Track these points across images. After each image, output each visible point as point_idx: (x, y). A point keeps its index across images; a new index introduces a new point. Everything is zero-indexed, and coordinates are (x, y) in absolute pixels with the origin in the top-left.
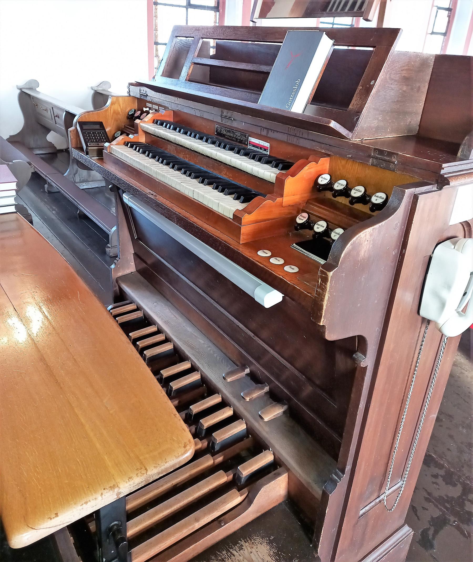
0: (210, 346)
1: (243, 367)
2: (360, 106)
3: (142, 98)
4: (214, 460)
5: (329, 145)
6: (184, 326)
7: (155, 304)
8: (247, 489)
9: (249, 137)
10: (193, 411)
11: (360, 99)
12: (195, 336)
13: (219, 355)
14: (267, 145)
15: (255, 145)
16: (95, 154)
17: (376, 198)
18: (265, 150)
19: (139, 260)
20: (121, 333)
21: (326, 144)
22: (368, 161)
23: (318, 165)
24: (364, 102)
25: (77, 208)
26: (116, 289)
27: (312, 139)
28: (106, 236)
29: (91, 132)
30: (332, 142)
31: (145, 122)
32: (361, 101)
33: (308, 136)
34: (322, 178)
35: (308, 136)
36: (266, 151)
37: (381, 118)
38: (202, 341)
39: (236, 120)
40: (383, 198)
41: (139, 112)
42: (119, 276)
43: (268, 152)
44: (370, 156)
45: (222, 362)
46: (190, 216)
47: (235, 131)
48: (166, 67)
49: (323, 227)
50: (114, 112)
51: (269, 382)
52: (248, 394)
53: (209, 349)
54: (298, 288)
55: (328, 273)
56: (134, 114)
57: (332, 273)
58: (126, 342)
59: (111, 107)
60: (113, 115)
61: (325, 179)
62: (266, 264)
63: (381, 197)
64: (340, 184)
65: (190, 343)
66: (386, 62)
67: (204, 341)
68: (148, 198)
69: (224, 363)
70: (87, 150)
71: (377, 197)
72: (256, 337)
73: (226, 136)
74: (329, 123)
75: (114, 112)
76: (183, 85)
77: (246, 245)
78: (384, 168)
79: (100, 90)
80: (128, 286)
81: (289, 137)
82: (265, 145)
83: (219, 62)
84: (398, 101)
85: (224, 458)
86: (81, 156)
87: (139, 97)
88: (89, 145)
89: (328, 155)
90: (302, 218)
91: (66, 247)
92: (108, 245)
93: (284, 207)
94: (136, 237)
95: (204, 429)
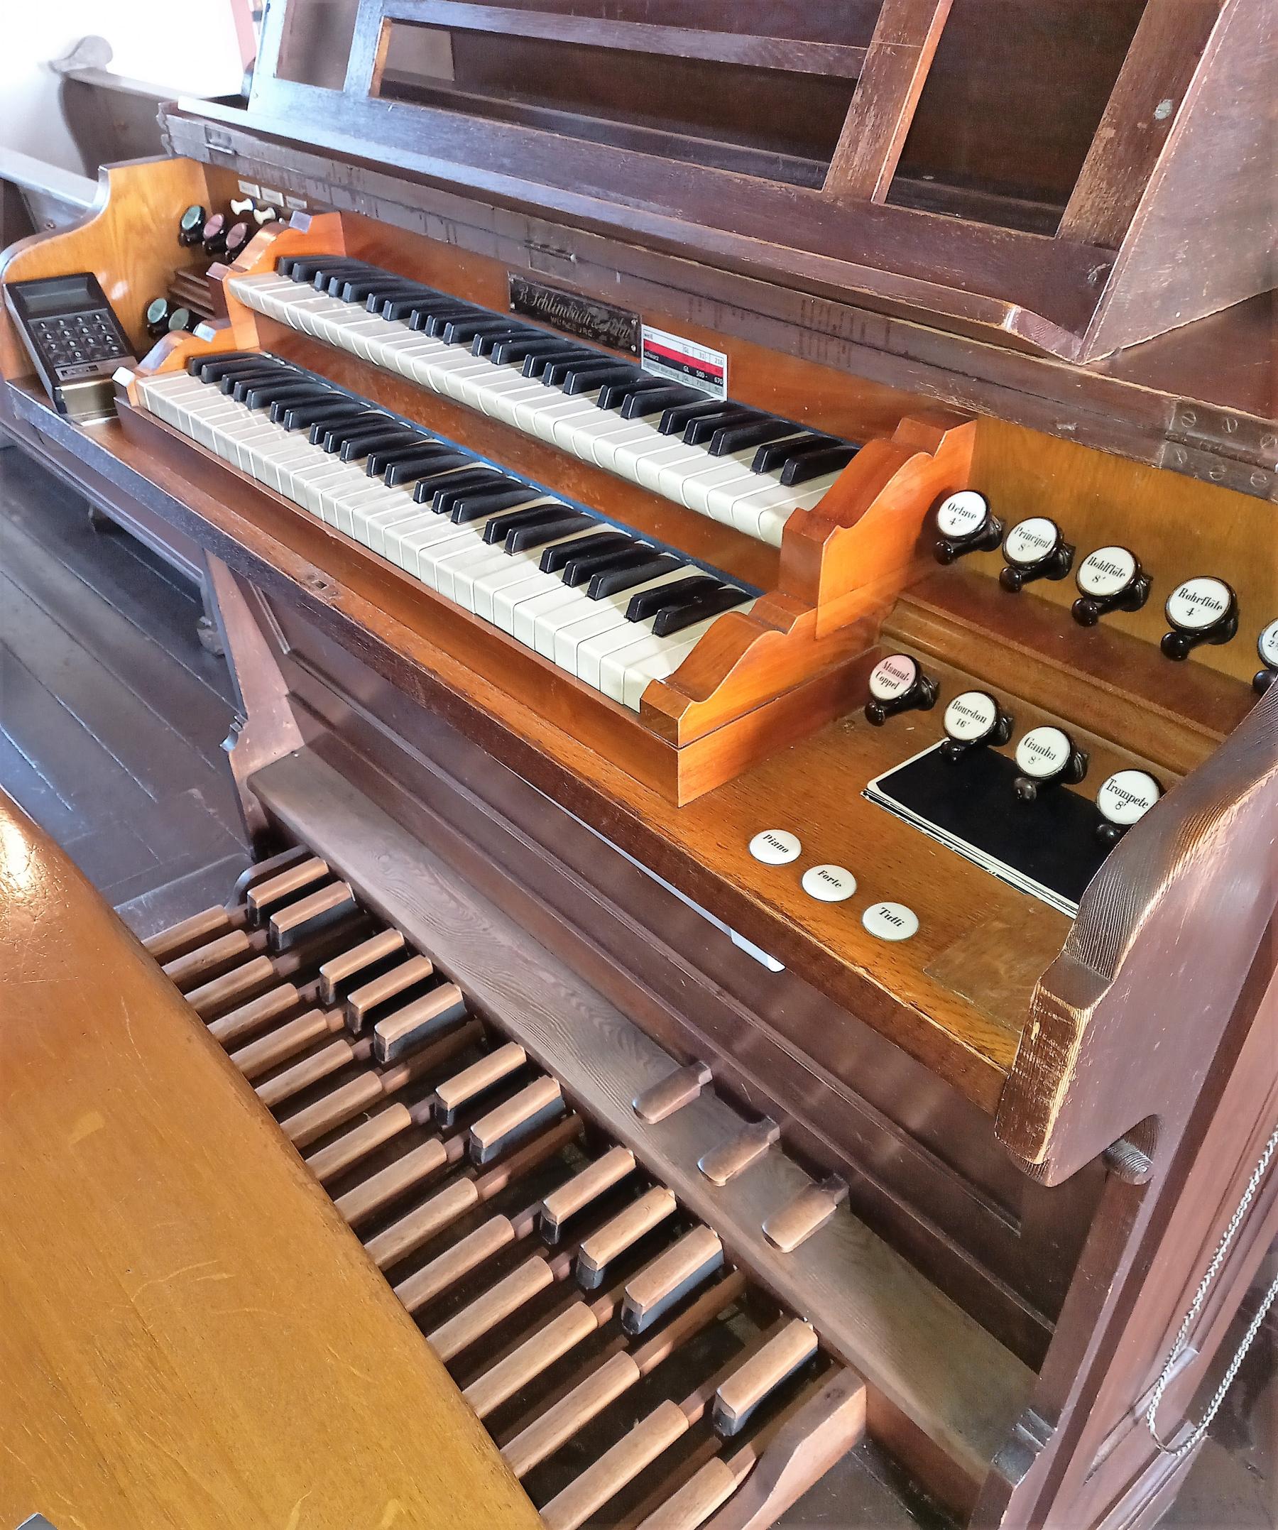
0: (575, 992)
1: (691, 1063)
2: (1111, 223)
3: (220, 161)
4: (639, 1364)
5: (979, 379)
6: (484, 930)
7: (385, 859)
8: (753, 1449)
9: (643, 326)
10: (556, 1217)
11: (1110, 185)
12: (526, 961)
13: (606, 1018)
15: (666, 358)
16: (92, 404)
17: (1190, 604)
19: (306, 716)
20: (300, 1181)
21: (965, 374)
22: (1151, 454)
23: (938, 458)
24: (1126, 198)
25: (85, 504)
26: (253, 810)
27: (907, 353)
29: (62, 322)
32: (1115, 193)
34: (953, 507)
37: (1185, 252)
38: (548, 975)
39: (588, 261)
40: (1217, 606)
41: (219, 219)
43: (722, 385)
44: (1158, 434)
45: (621, 1045)
46: (471, 681)
47: (585, 301)
48: (288, 36)
49: (983, 720)
50: (130, 227)
51: (779, 1116)
52: (720, 1162)
53: (574, 1001)
54: (938, 1026)
55: (1074, 1012)
56: (202, 226)
57: (1088, 1013)
59: (114, 212)
60: (127, 240)
61: (966, 514)
63: (1207, 602)
64: (1028, 537)
65: (513, 988)
66: (1223, 9)
67: (554, 975)
68: (306, 598)
69: (626, 1048)
71: (1194, 598)
72: (729, 997)
73: (553, 319)
75: (130, 227)
76: (361, 113)
77: (702, 807)
78: (1220, 484)
79: (78, 68)
81: (806, 339)
82: (707, 361)
83: (488, 15)
84: (1246, 170)
85: (410, 1076)
87: (207, 160)
88: (59, 374)
90: (894, 679)
91: (75, 635)
92: (203, 619)
93: (823, 638)
94: (286, 648)
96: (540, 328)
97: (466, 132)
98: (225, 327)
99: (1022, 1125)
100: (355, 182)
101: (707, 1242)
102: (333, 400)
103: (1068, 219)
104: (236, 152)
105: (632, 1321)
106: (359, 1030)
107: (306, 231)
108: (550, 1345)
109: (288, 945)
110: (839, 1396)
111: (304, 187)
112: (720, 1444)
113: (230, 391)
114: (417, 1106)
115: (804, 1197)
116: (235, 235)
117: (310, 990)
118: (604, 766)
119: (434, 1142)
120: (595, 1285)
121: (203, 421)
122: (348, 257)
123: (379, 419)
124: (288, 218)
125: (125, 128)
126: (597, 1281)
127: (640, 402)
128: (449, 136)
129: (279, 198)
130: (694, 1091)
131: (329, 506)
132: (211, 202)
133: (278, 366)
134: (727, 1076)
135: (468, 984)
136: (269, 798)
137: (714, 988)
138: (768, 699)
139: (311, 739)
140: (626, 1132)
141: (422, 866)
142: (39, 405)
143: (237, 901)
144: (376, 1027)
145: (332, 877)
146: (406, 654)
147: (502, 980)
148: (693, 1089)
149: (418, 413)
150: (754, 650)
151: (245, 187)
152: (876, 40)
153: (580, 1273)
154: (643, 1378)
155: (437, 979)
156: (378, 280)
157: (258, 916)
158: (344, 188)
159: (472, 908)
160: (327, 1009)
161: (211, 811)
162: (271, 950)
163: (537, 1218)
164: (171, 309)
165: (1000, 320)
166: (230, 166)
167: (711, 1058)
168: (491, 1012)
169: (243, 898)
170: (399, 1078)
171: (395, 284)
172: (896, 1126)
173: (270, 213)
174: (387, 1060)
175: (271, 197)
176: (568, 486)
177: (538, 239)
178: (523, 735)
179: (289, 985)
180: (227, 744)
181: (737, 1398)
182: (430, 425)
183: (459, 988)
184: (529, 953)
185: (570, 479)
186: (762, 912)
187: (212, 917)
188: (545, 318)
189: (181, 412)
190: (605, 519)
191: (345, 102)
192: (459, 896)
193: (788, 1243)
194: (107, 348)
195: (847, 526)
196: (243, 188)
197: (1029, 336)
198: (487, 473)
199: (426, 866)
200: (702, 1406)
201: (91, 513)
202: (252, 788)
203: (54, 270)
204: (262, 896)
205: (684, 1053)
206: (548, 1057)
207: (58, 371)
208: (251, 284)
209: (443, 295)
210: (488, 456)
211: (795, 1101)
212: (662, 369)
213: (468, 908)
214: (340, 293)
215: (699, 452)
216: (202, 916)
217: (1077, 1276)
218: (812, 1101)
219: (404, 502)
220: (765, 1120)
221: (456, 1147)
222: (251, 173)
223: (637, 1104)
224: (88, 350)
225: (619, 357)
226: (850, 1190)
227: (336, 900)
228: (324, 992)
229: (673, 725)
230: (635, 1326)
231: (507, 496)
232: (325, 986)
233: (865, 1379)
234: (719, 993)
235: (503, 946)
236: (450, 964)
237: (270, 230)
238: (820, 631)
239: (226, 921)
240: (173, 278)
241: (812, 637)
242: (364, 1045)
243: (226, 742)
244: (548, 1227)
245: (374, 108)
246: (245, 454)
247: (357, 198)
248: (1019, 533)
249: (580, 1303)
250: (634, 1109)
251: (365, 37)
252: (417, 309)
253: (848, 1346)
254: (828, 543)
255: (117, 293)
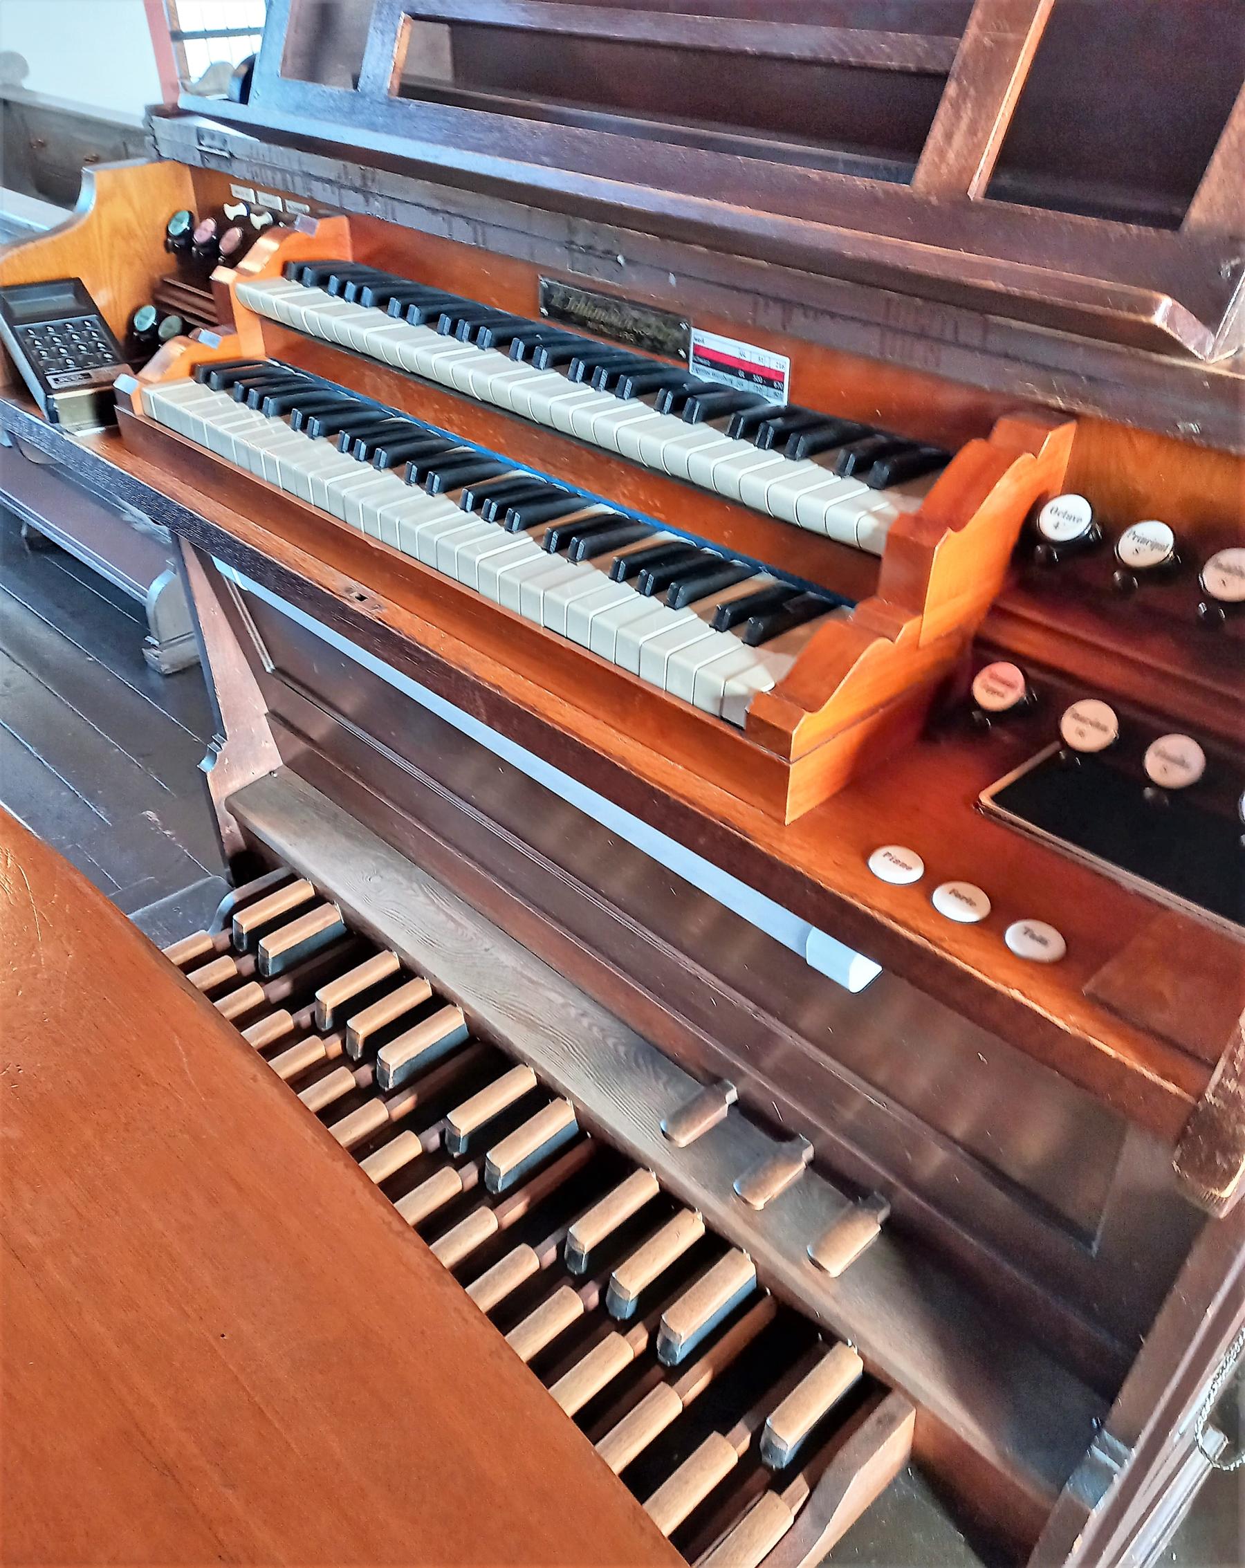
0: (585, 1012)
1: (714, 1081)
3: (213, 164)
6: (486, 950)
7: (376, 879)
9: (693, 330)
12: (532, 982)
14: (779, 362)
16: (86, 414)
18: (769, 382)
19: (285, 733)
25: (19, 522)
28: (138, 609)
29: (50, 329)
30: (1101, 367)
31: (248, 274)
33: (984, 338)
34: (1056, 511)
35: (984, 338)
36: (773, 387)
41: (210, 225)
42: (234, 790)
45: (638, 1066)
49: (1105, 729)
51: (812, 1133)
52: (758, 1185)
53: (585, 1022)
58: (427, 1274)
59: (99, 215)
60: (112, 246)
62: (927, 928)
65: (521, 1009)
67: (563, 996)
70: (50, 408)
74: (1149, 307)
75: (115, 231)
77: (809, 823)
80: (271, 824)
82: (767, 365)
86: (30, 428)
87: (198, 163)
89: (1068, 415)
90: (1000, 688)
92: (149, 639)
94: (269, 666)
95: (631, 1299)
96: (576, 333)
97: (500, 130)
98: (228, 333)
99: (1211, 1158)
100: (369, 183)
101: (742, 1266)
102: (352, 408)
103: (1196, 213)
104: (231, 154)
105: (670, 1351)
106: (359, 1056)
107: (313, 236)
108: (588, 1380)
109: (278, 970)
110: (890, 1422)
111: (310, 190)
112: (769, 1477)
113: (245, 398)
114: (425, 1134)
115: (848, 1219)
116: (229, 240)
117: (304, 1017)
118: (697, 783)
119: (448, 1170)
120: (628, 1315)
121: (221, 429)
122: (355, 262)
123: (405, 427)
124: (290, 223)
125: (43, 145)
126: (628, 1310)
127: (704, 408)
128: (481, 136)
129: (277, 203)
130: (722, 1112)
131: (370, 516)
132: (198, 209)
133: (286, 373)
134: (757, 1095)
135: (473, 1006)
136: (250, 820)
137: (749, 1006)
138: (872, 711)
139: (290, 757)
140: (651, 1156)
141: (415, 886)
142: (26, 414)
143: (221, 925)
144: (379, 1052)
145: (319, 899)
146: (465, 669)
147: (508, 1001)
148: (721, 1109)
149: (450, 422)
150: (865, 660)
151: (237, 191)
152: (972, 30)
153: (612, 1302)
154: (687, 1410)
155: (437, 1002)
156: (395, 285)
157: (245, 942)
158: (356, 190)
159: (471, 927)
160: (324, 1035)
161: (167, 833)
162: (259, 975)
163: (560, 1248)
164: (160, 318)
165: (1150, 311)
166: (224, 168)
167: (737, 1075)
168: (500, 1035)
169: (228, 922)
170: (405, 1104)
171: (413, 290)
172: (955, 1145)
173: (267, 218)
174: (391, 1086)
175: (268, 201)
176: (624, 494)
177: (580, 240)
178: (604, 751)
179: (283, 1011)
180: (205, 765)
181: (788, 1429)
182: (464, 433)
183: (460, 1009)
184: (535, 972)
185: (625, 486)
186: (896, 935)
187: (195, 943)
188: (582, 322)
189: (193, 419)
190: (666, 527)
191: (361, 102)
192: (456, 916)
193: (836, 1265)
194: (99, 355)
195: (957, 529)
196: (237, 192)
197: (1176, 331)
198: (531, 482)
199: (421, 887)
200: (749, 1437)
201: (24, 532)
202: (231, 810)
203: (38, 274)
204: (248, 920)
205: (705, 1071)
206: (562, 1078)
207: (50, 379)
208: (261, 289)
209: (465, 300)
210: (528, 463)
211: (830, 1118)
212: (714, 374)
213: (466, 928)
214: (358, 298)
215: (775, 458)
216: (186, 942)
217: (1171, 1300)
218: (848, 1115)
219: (453, 511)
220: (798, 1141)
221: (470, 1175)
222: (249, 177)
223: (666, 1127)
224: (80, 358)
225: (665, 362)
226: (892, 1212)
227: (327, 922)
228: (320, 1017)
229: (787, 738)
230: (674, 1356)
231: (560, 505)
232: (322, 1012)
233: (915, 1403)
234: (756, 1013)
235: (507, 967)
236: (452, 985)
237: (274, 237)
238: (923, 640)
239: (211, 946)
240: (159, 284)
241: (916, 646)
242: (366, 1072)
243: (203, 762)
244: (574, 1255)
245: (395, 107)
246: (270, 462)
247: (371, 199)
248: (1132, 536)
249: (614, 1334)
250: (663, 1132)
251: (382, 33)
252: (447, 313)
253: (899, 1371)
254: (940, 548)
255: (101, 299)
